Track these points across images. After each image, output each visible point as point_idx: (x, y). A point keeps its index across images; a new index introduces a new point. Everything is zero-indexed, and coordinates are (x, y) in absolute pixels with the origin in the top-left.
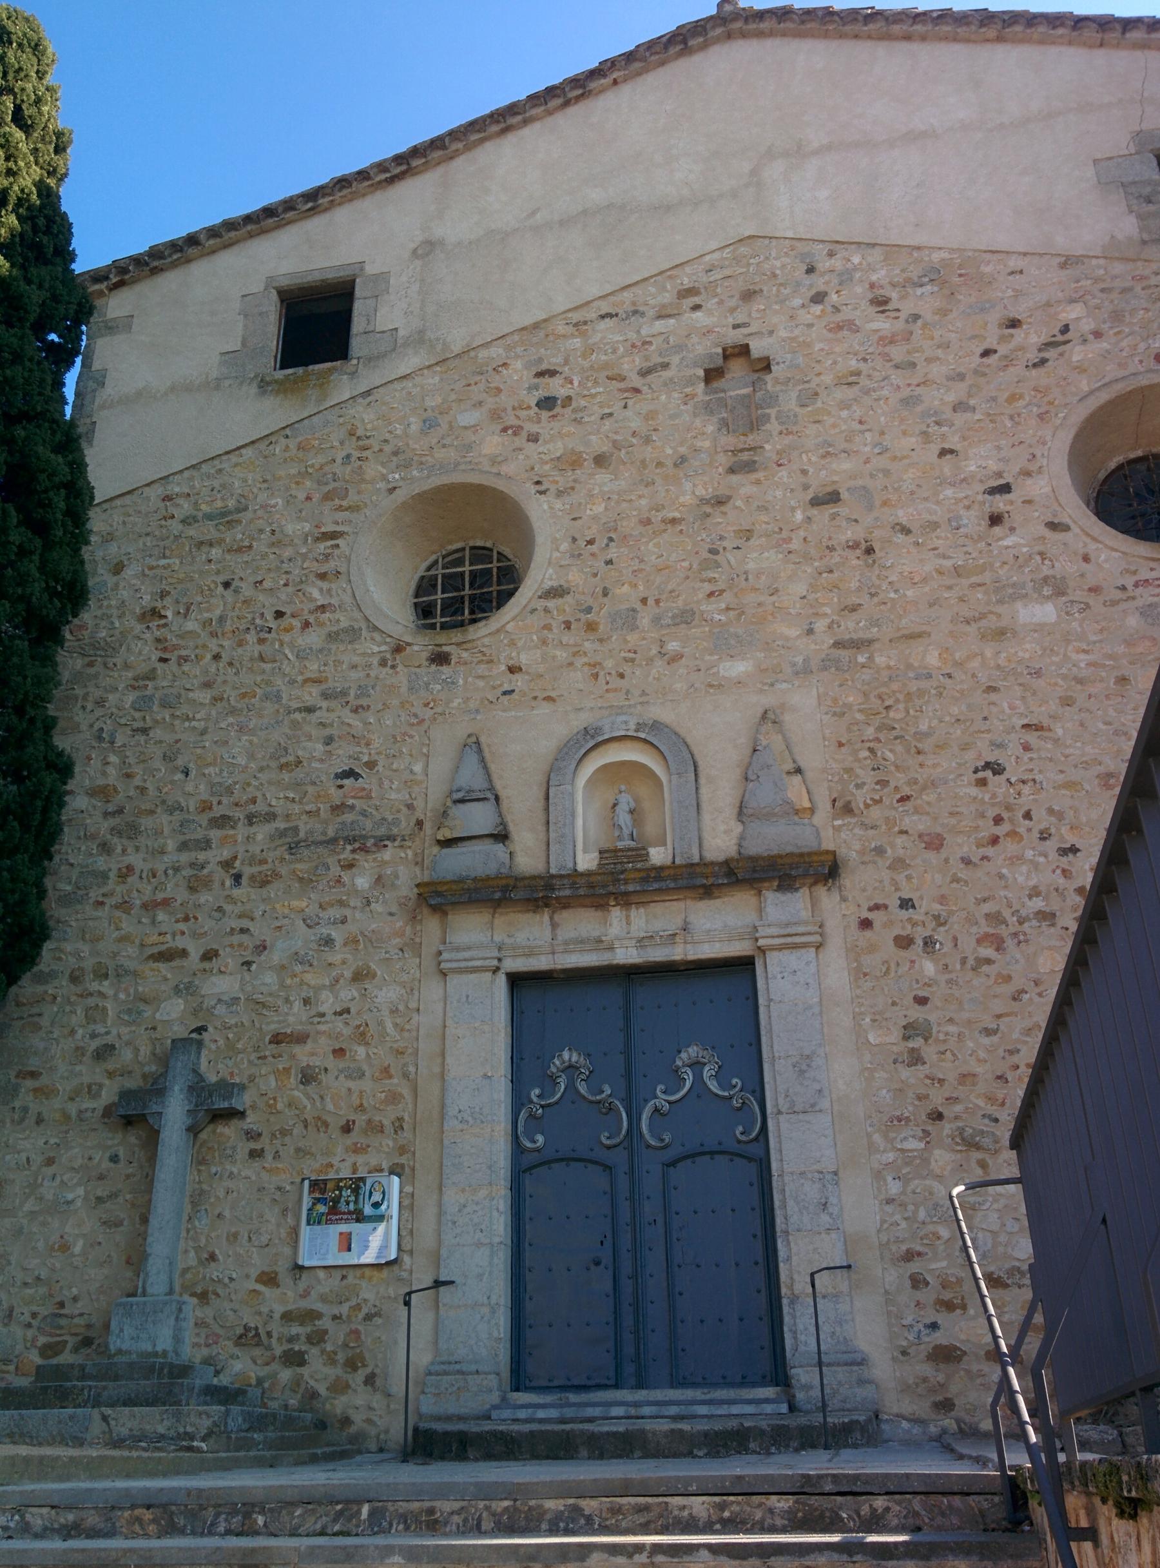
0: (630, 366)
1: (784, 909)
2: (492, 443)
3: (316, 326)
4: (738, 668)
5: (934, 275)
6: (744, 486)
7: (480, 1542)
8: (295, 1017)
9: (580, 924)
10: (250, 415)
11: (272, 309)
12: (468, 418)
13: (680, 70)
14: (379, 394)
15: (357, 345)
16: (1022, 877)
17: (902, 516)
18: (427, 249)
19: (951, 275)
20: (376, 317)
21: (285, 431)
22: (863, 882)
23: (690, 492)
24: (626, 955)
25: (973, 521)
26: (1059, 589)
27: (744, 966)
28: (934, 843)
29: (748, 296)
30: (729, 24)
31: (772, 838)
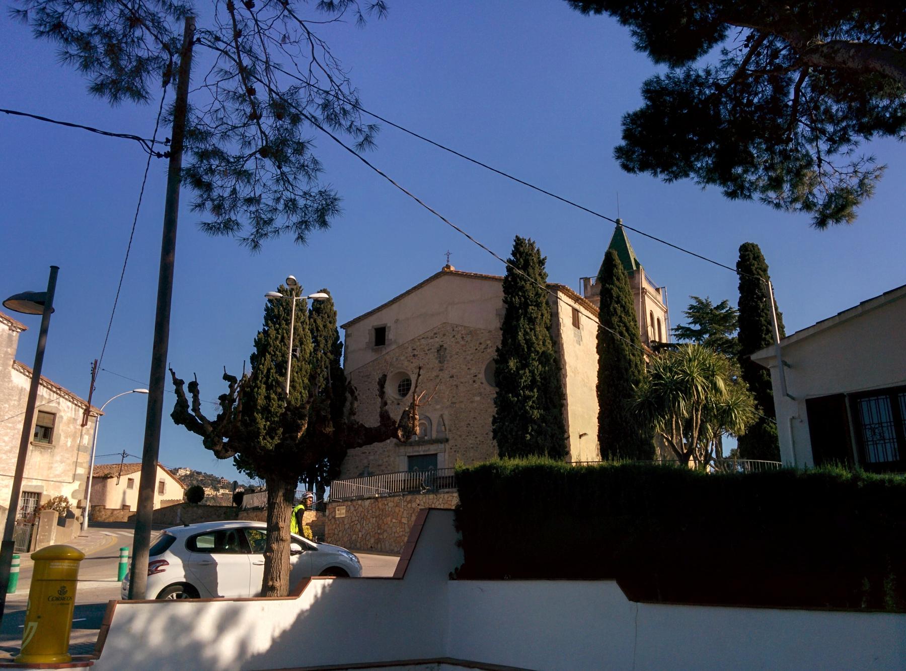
0: (426, 349)
1: (442, 446)
2: (406, 363)
3: (380, 335)
4: (438, 407)
5: (470, 333)
6: (441, 373)
7: (851, 428)
8: (380, 462)
9: (416, 448)
10: (370, 356)
11: (373, 332)
12: (403, 358)
13: (434, 283)
14: (391, 350)
15: (386, 342)
16: (470, 442)
17: (462, 380)
18: (397, 321)
19: (472, 333)
20: (390, 336)
21: (376, 360)
22: (451, 442)
23: (434, 374)
24: (422, 453)
25: (471, 382)
26: (480, 394)
27: (436, 455)
28: (460, 436)
29: (444, 335)
30: (347, 669)
31: (442, 436)
